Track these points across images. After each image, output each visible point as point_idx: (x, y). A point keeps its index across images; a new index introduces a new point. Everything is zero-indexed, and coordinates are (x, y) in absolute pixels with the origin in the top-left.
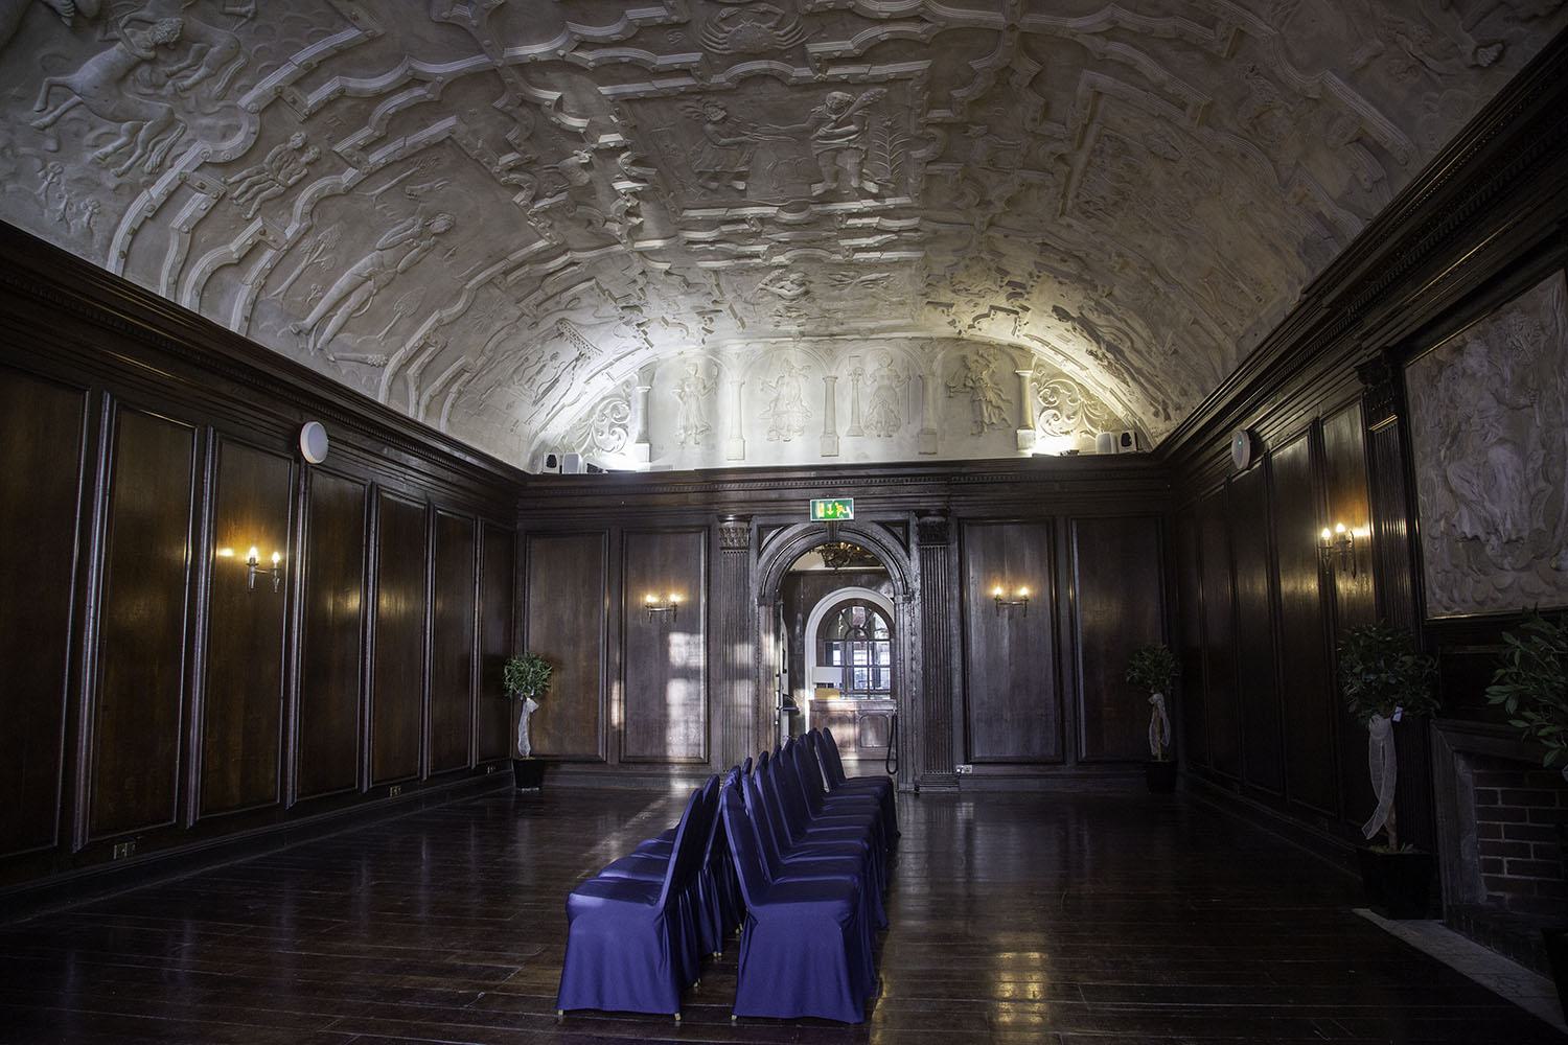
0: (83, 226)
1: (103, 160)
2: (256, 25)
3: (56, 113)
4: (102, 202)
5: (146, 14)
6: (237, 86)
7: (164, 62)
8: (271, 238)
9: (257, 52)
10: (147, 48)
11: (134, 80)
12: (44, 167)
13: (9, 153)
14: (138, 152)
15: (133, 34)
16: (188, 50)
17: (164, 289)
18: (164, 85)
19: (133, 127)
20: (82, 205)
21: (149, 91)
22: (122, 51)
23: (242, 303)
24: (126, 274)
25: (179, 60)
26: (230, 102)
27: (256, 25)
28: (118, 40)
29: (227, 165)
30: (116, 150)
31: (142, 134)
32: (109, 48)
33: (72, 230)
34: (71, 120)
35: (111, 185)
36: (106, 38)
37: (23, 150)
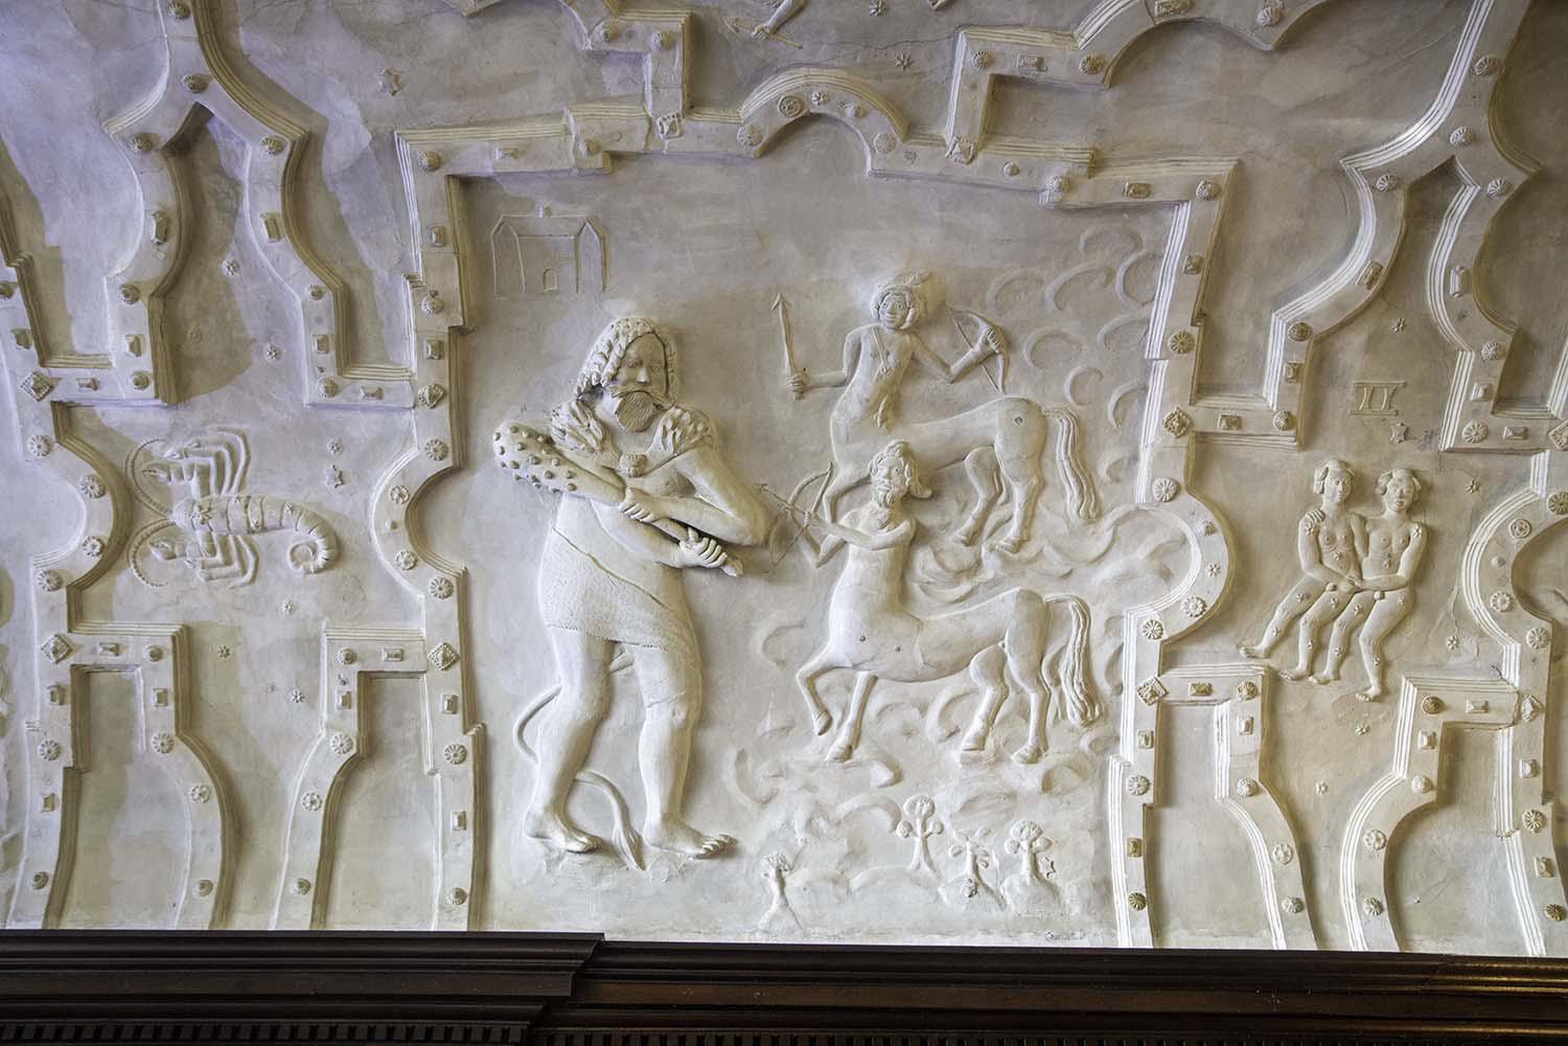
0: (1024, 885)
1: (982, 748)
2: (1025, 353)
3: (852, 716)
4: (1041, 821)
5: (844, 475)
6: (1102, 471)
7: (946, 527)
8: (1469, 707)
9: (1072, 390)
10: (890, 522)
11: (924, 590)
12: (897, 816)
13: (822, 824)
14: (1034, 700)
15: (855, 519)
16: (963, 478)
17: (1280, 932)
18: (979, 563)
19: (986, 663)
20: (1007, 849)
21: (965, 587)
22: (858, 556)
23: (1523, 880)
24: (1417, 919)
25: (964, 507)
26: (1119, 512)
27: (1025, 353)
28: (843, 544)
29: (1212, 623)
30: (990, 721)
31: (1013, 666)
32: (843, 564)
33: (1009, 901)
34: (881, 713)
35: (1031, 780)
36: (822, 553)
37: (844, 808)
